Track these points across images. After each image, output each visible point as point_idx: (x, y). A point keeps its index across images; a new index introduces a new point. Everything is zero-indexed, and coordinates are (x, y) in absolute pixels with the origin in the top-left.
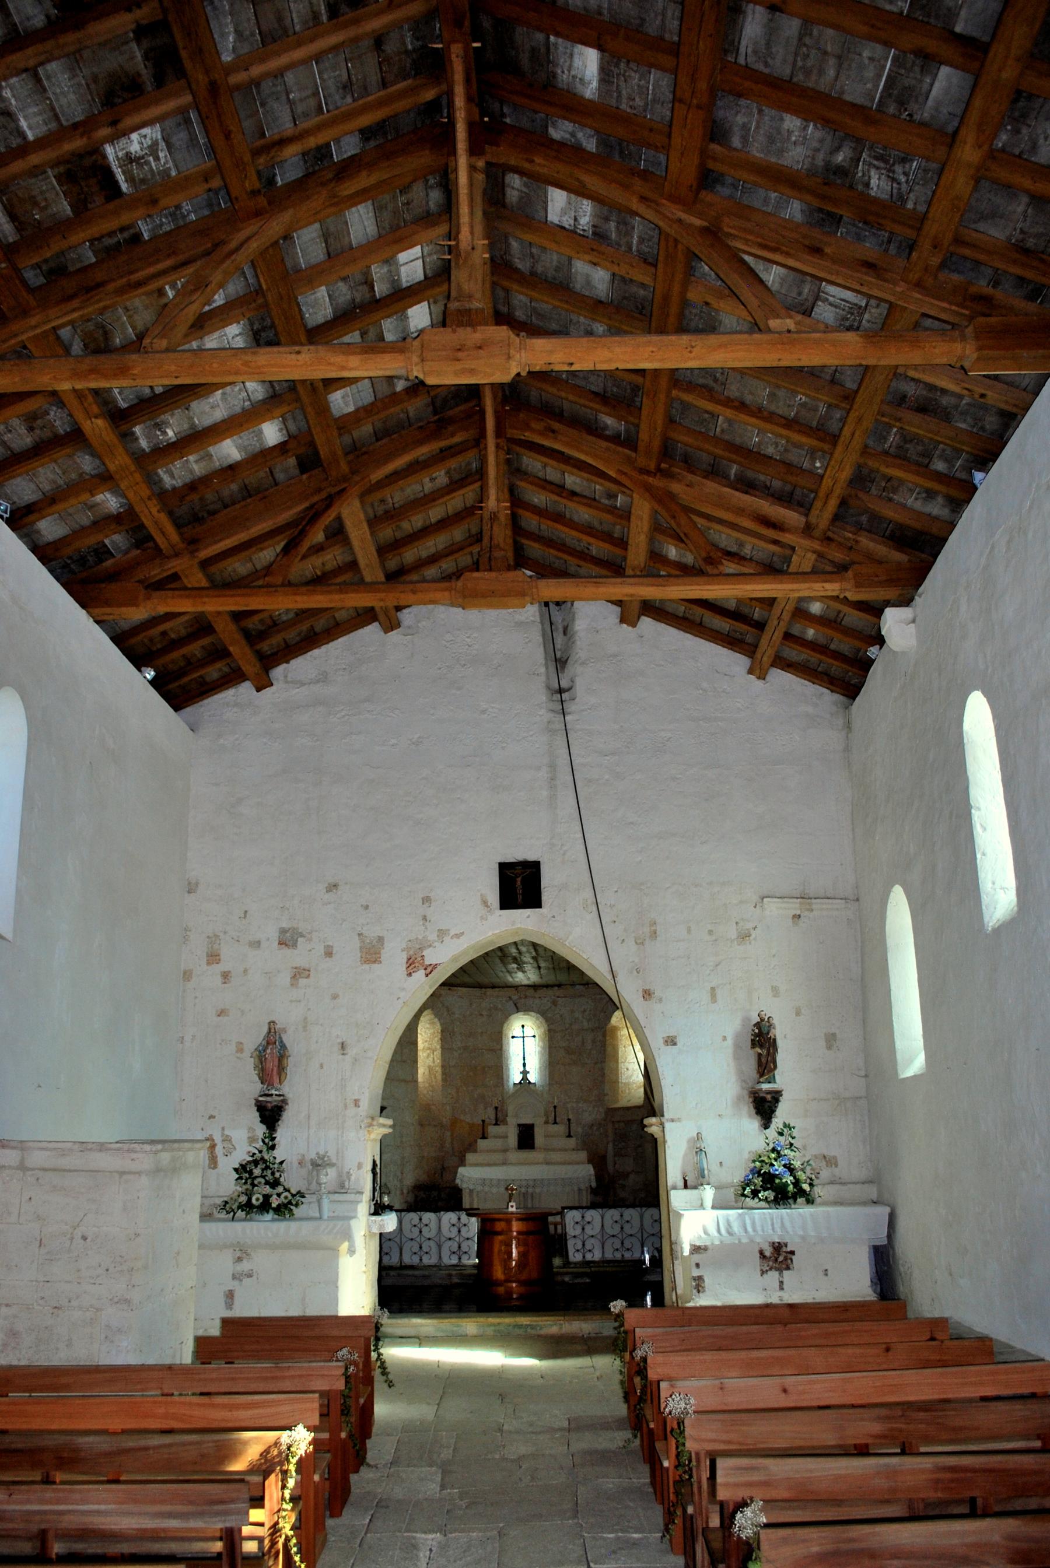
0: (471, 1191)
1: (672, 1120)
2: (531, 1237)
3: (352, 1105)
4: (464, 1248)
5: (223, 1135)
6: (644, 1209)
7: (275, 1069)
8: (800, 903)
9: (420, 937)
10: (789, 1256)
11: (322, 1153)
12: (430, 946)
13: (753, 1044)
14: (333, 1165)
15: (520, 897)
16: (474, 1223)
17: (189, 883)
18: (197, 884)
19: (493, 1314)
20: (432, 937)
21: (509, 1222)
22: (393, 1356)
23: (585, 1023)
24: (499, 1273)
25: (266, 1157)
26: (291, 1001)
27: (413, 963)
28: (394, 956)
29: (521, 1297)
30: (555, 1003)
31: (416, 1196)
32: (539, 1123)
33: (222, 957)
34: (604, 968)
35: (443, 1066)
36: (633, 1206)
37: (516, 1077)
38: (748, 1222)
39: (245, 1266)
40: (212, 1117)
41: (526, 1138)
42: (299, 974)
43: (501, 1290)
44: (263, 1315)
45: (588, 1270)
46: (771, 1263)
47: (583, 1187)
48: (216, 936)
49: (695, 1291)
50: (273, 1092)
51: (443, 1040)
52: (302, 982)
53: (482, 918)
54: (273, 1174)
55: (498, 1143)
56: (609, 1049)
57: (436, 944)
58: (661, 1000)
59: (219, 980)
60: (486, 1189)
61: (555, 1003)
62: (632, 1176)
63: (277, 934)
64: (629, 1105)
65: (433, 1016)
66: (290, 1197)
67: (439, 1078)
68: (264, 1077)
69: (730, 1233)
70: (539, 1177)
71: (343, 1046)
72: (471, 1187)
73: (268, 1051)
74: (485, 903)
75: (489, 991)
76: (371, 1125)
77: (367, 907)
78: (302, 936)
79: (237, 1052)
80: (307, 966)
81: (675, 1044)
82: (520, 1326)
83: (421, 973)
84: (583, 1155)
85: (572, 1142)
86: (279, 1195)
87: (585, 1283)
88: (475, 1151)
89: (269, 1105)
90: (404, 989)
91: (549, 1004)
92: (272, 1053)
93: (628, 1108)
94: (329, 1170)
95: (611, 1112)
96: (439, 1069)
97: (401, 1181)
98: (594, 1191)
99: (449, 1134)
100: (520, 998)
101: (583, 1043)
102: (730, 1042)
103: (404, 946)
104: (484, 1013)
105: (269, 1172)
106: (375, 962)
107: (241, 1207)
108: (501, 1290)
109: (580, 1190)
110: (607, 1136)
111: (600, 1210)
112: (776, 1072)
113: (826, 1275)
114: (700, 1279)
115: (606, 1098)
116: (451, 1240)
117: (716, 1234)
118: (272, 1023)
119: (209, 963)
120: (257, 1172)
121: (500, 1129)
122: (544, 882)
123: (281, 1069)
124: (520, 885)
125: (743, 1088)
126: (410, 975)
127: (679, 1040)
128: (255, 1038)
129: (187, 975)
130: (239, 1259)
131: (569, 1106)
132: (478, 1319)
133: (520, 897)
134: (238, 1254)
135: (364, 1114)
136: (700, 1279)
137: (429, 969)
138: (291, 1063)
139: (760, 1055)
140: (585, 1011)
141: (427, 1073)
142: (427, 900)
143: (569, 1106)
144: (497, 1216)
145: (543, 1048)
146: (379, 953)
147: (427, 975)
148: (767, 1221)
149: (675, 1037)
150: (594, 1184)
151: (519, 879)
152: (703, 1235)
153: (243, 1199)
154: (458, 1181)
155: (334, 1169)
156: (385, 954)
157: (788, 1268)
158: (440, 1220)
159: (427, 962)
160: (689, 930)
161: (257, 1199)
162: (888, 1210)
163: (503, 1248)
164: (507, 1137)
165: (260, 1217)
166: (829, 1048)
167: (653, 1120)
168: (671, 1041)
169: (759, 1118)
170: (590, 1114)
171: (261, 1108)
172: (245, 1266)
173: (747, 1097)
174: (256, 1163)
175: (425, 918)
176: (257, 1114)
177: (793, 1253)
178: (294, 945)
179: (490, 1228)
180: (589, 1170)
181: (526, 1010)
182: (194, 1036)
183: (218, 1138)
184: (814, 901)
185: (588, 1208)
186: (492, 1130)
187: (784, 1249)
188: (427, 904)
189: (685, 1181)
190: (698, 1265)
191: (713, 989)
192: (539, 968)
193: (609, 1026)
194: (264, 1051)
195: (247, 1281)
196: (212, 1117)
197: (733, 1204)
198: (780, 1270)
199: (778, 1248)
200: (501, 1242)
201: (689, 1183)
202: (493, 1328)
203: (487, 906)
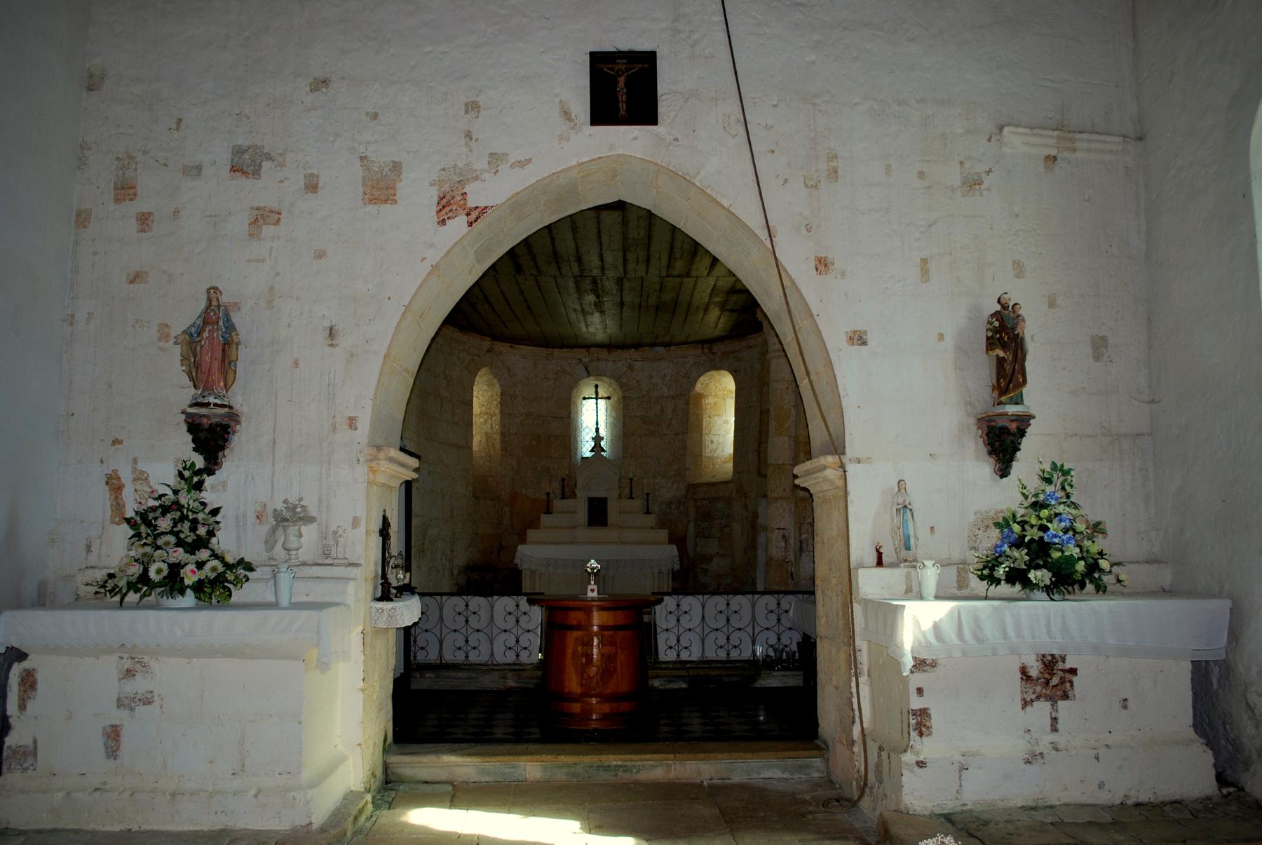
0: (533, 572)
1: (859, 461)
2: (621, 634)
3: (346, 426)
4: (524, 641)
5: (134, 470)
6: (706, 597)
7: (216, 365)
8: (1058, 137)
9: (461, 164)
10: (1068, 676)
11: (293, 499)
12: (477, 178)
13: (991, 344)
14: (311, 520)
15: (623, 107)
16: (536, 615)
17: (91, 76)
18: (103, 77)
19: (567, 747)
20: (481, 164)
21: (588, 611)
23: (665, 390)
24: (573, 684)
25: (183, 501)
26: (249, 261)
27: (449, 204)
28: (418, 193)
29: (604, 717)
30: (630, 368)
32: (612, 496)
33: (139, 190)
34: (754, 221)
35: (502, 434)
36: (716, 592)
37: (586, 449)
38: (1009, 621)
39: (139, 685)
40: (116, 442)
41: (598, 513)
42: (262, 218)
43: (576, 708)
45: (684, 673)
46: (1038, 688)
48: (131, 157)
49: (914, 734)
50: (212, 400)
51: (503, 404)
52: (268, 230)
53: (561, 137)
54: (193, 529)
57: (486, 175)
58: (843, 274)
59: (133, 225)
61: (630, 368)
62: (715, 560)
63: (229, 156)
64: (714, 480)
66: (221, 569)
67: (498, 446)
68: (196, 371)
69: (979, 639)
71: (331, 332)
72: (533, 568)
73: (206, 335)
74: (566, 114)
75: (557, 352)
76: (375, 459)
77: (375, 116)
78: (269, 158)
79: (159, 339)
80: (275, 206)
81: (864, 343)
82: (607, 768)
83: (462, 220)
84: (663, 534)
85: (651, 520)
86: (200, 565)
87: (680, 690)
89: (205, 421)
90: (432, 245)
92: (211, 338)
93: (714, 484)
94: (304, 529)
95: (693, 488)
96: (498, 437)
98: (675, 575)
99: (507, 509)
102: (949, 342)
103: (434, 177)
105: (187, 525)
106: (386, 201)
107: (132, 586)
108: (576, 708)
109: (660, 573)
111: (700, 597)
112: (1025, 390)
113: (1125, 707)
114: (923, 713)
116: (506, 634)
117: (956, 641)
118: (213, 291)
119: (117, 200)
120: (164, 524)
122: (662, 87)
123: (227, 363)
124: (623, 88)
125: (969, 414)
126: (443, 222)
127: (869, 338)
128: (187, 315)
129: (82, 218)
130: (130, 673)
131: (645, 481)
132: (544, 757)
133: (623, 107)
134: (128, 664)
135: (365, 440)
136: (923, 713)
137: (474, 215)
138: (244, 357)
139: (1000, 361)
141: (484, 440)
142: (472, 107)
143: (645, 481)
144: (571, 603)
145: (615, 418)
146: (394, 188)
147: (470, 224)
148: (1040, 621)
149: (866, 332)
150: (677, 567)
151: (622, 80)
152: (934, 641)
153: (136, 570)
154: (517, 561)
155: (314, 526)
156: (403, 190)
157: (1065, 697)
158: (492, 607)
159: (471, 204)
160: (888, 170)
161: (159, 571)
162: (1222, 606)
163: (579, 649)
165: (171, 602)
166: (1097, 358)
167: (830, 459)
168: (858, 339)
169: (992, 460)
170: (668, 491)
171: (194, 427)
172: (139, 685)
173: (974, 428)
174: (165, 510)
175: (469, 135)
176: (190, 437)
177: (1073, 671)
178: (257, 173)
179: (560, 619)
180: (673, 550)
181: (599, 374)
182: (90, 315)
183: (126, 476)
184: (1078, 136)
185: (451, 594)
186: (558, 504)
187: (1060, 665)
188: (473, 114)
189: (880, 555)
190: (920, 691)
191: (924, 261)
192: (622, 304)
194: (199, 334)
195: (141, 710)
196: (116, 442)
197: (956, 591)
198: (1053, 700)
199: (1050, 663)
200: (576, 639)
201: (885, 559)
202: (565, 770)
203: (570, 119)
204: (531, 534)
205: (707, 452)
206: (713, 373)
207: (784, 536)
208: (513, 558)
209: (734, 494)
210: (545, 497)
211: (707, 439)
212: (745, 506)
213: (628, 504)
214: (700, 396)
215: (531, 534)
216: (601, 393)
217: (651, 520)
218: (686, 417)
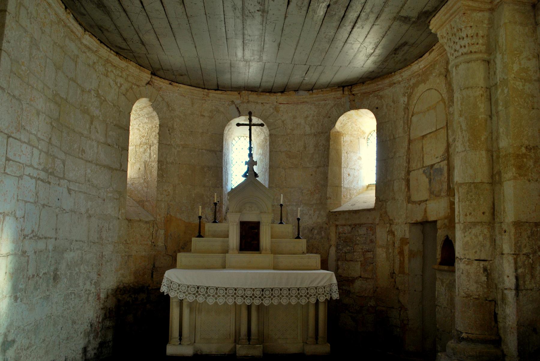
22: (263, 154)
23: (308, 129)
30: (276, 109)
31: (119, 301)
35: (159, 162)
41: (250, 238)
44: (375, 128)
47: (322, 299)
51: (161, 134)
55: (217, 243)
56: (332, 153)
60: (201, 299)
65: (151, 109)
67: (155, 173)
70: (269, 286)
75: (212, 93)
88: (189, 251)
91: (272, 110)
96: (155, 165)
97: (97, 284)
99: (162, 232)
100: (243, 102)
101: (305, 148)
104: (206, 114)
110: (329, 239)
115: (329, 201)
121: (219, 227)
140: (307, 117)
154: (164, 289)
164: (227, 236)
186: (209, 227)
193: (333, 131)
204: (181, 257)
205: (346, 183)
206: (353, 112)
207: (485, 270)
208: (160, 283)
209: (377, 221)
210: (197, 221)
211: (345, 172)
212: (391, 232)
213: (279, 228)
214: (339, 135)
215: (181, 257)
216: (255, 120)
217: (302, 243)
218: (325, 154)
